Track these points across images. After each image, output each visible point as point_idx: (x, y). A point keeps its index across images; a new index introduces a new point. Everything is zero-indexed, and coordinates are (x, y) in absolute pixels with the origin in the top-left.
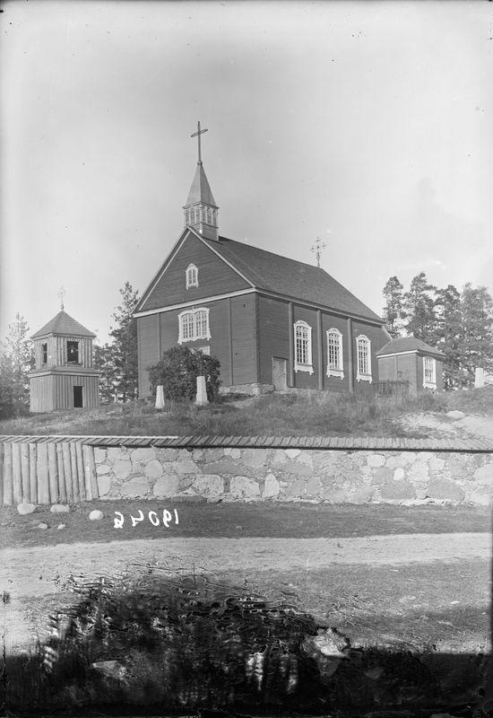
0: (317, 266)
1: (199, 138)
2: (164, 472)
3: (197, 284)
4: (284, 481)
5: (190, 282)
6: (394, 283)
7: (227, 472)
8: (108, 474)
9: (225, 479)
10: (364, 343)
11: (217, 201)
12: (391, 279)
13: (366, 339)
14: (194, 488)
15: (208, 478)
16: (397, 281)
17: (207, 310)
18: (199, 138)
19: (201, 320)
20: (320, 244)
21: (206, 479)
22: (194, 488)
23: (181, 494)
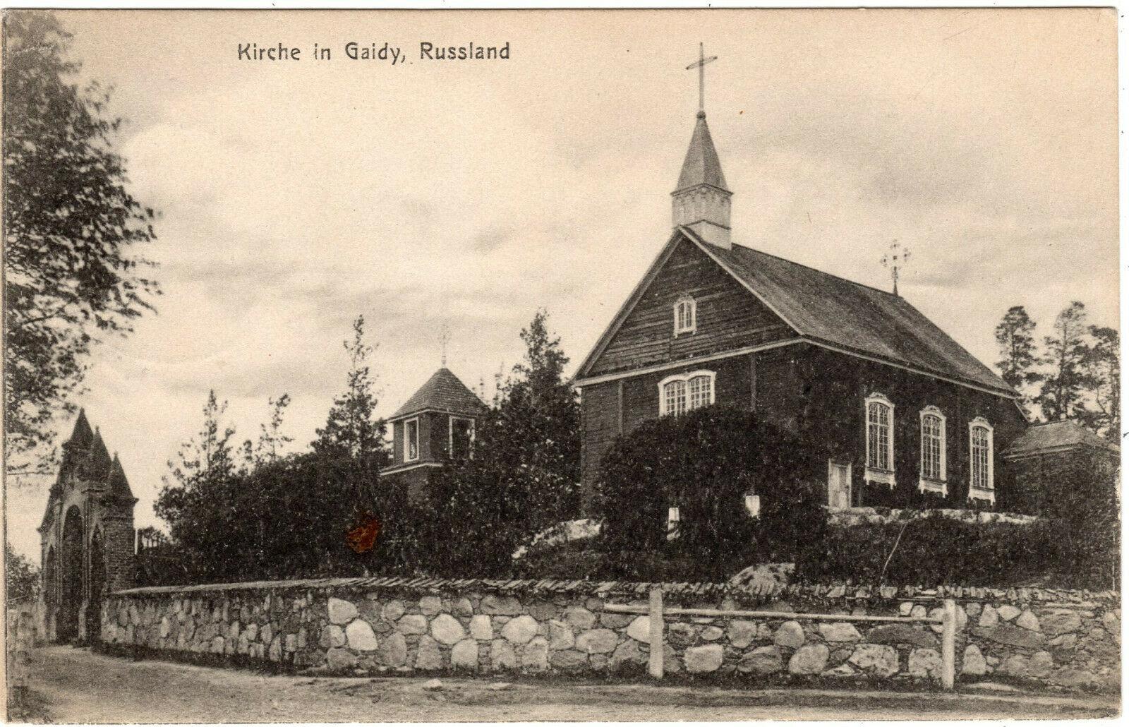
0: (891, 291)
1: (701, 72)
2: (807, 638)
3: (693, 328)
4: (993, 655)
5: (681, 326)
6: (1017, 320)
7: (906, 641)
8: (719, 641)
9: (900, 650)
10: (981, 431)
11: (730, 184)
12: (1012, 310)
13: (985, 425)
14: (851, 664)
15: (876, 649)
16: (1023, 314)
17: (712, 375)
18: (701, 72)
19: (701, 392)
20: (899, 252)
21: (871, 652)
22: (851, 664)
23: (831, 672)
